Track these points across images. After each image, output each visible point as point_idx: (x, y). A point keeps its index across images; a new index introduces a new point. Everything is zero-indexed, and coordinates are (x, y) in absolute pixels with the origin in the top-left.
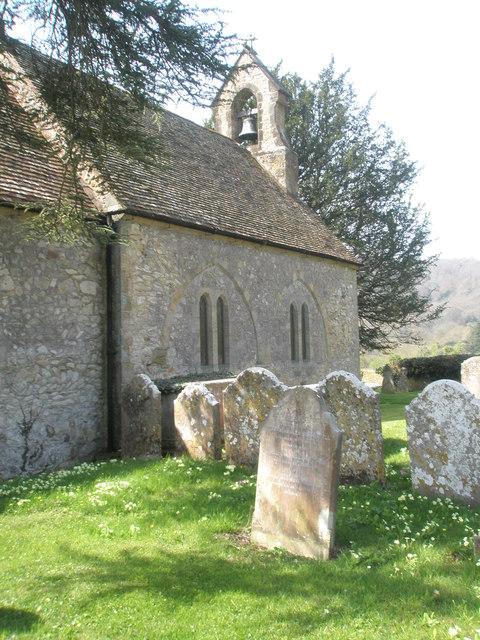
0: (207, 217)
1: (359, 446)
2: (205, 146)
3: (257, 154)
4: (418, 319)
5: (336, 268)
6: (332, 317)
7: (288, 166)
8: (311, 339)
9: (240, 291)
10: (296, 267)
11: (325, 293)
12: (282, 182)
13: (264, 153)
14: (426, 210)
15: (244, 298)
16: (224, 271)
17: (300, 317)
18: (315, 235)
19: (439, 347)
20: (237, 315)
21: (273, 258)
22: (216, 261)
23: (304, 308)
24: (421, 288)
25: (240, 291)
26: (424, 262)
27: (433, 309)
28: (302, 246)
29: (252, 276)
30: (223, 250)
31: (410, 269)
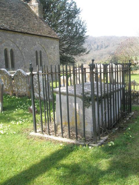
0: (6, 26)
1: (24, 88)
2: (11, 3)
3: (30, 6)
4: (83, 54)
5: (51, 40)
6: (50, 54)
7: (39, 10)
8: (43, 60)
9: (18, 47)
10: (37, 40)
11: (48, 47)
12: (37, 14)
13: (32, 5)
14: (85, 22)
15: (19, 49)
16: (12, 42)
17: (39, 54)
18: (46, 29)
19: (102, 62)
20: (17, 53)
21: (29, 38)
22: (9, 39)
23: (40, 52)
24: (85, 46)
25: (18, 47)
26: (84, 38)
27: (87, 51)
28: (39, 34)
29: (22, 43)
30: (12, 36)
31: (79, 38)
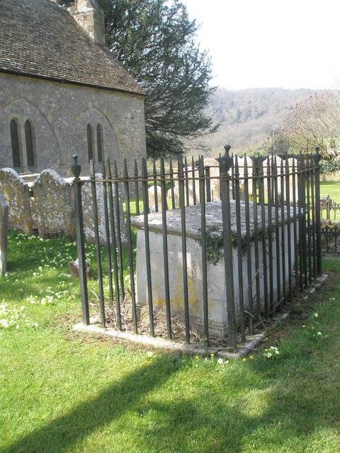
0: (14, 64)
1: (59, 215)
2: (27, 8)
3: (74, 14)
4: (203, 133)
5: (126, 98)
6: (123, 132)
7: (96, 23)
8: (105, 148)
9: (44, 116)
10: (92, 99)
11: (117, 116)
12: (92, 35)
13: (78, 13)
14: (209, 55)
15: (47, 120)
16: (30, 102)
17: (95, 133)
18: (112, 72)
19: (250, 151)
20: (41, 131)
21: (71, 92)
22: (22, 95)
23: (99, 127)
24: (207, 112)
25: (44, 116)
26: (206, 92)
27: (213, 125)
28: (96, 83)
29: (53, 105)
30: (28, 87)
31: (194, 93)
